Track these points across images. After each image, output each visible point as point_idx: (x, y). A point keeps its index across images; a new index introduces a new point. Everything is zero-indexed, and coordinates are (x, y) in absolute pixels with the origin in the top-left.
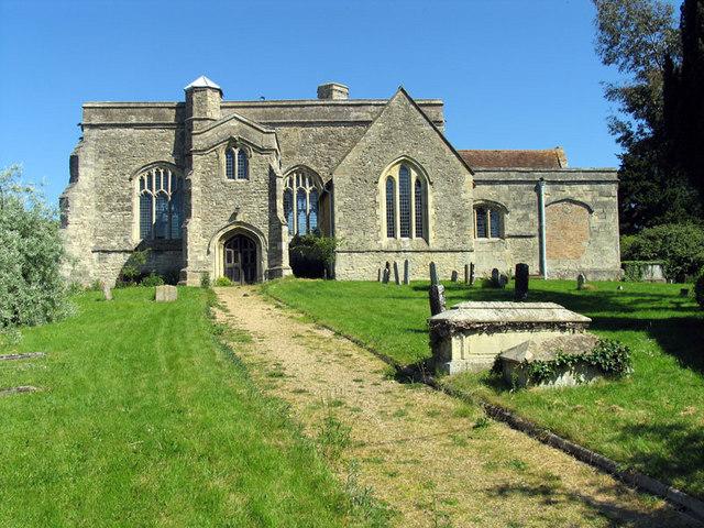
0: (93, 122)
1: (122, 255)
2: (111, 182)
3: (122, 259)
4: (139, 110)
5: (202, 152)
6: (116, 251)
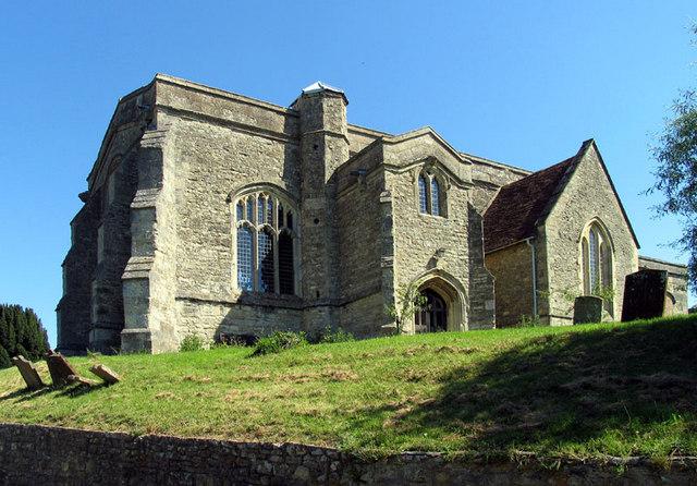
0: (173, 105)
1: (218, 308)
2: (199, 200)
3: (217, 315)
4: (239, 106)
5: (395, 168)
6: (210, 302)
